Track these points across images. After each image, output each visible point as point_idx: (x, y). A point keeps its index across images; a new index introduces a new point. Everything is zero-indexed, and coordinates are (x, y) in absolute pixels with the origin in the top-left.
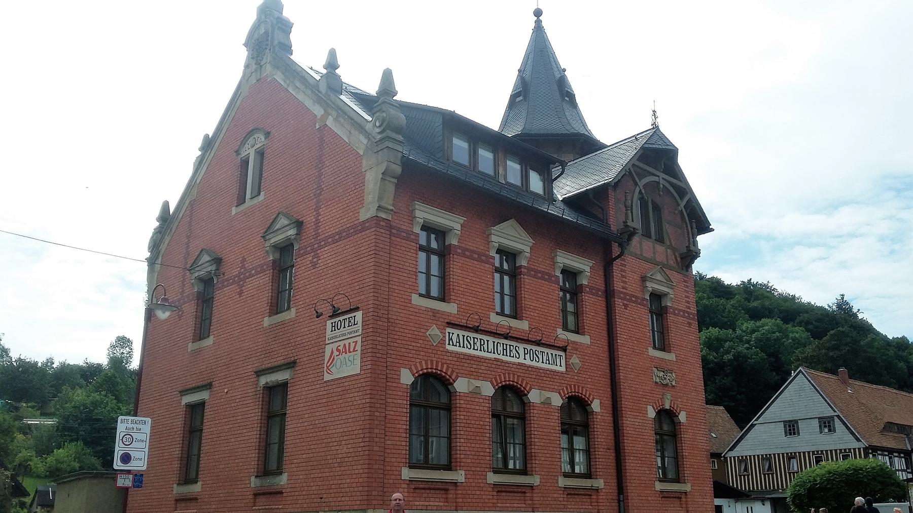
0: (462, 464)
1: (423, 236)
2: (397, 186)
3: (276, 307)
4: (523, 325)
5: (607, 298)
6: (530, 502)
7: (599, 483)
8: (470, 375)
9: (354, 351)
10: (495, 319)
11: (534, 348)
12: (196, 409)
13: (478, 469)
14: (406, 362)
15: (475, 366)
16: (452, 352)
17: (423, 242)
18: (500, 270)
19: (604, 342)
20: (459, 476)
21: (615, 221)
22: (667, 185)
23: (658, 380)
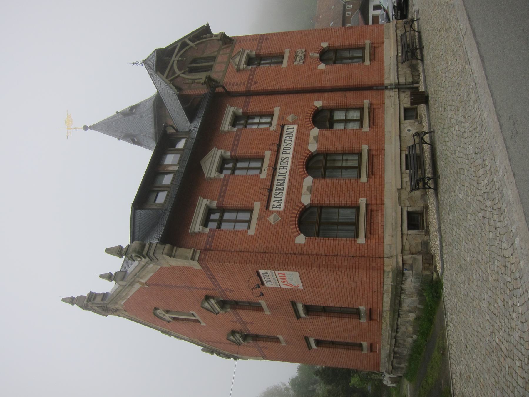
0: (356, 200)
1: (227, 172)
2: (180, 246)
3: (258, 308)
4: (268, 154)
5: (251, 95)
6: (379, 151)
7: (366, 103)
8: (299, 194)
10: (263, 176)
11: (282, 147)
12: (318, 343)
13: (358, 188)
14: (291, 239)
15: (294, 190)
16: (285, 206)
17: (228, 172)
18: (234, 169)
19: (279, 98)
20: (363, 202)
21: (203, 90)
22: (179, 55)
23: (302, 61)
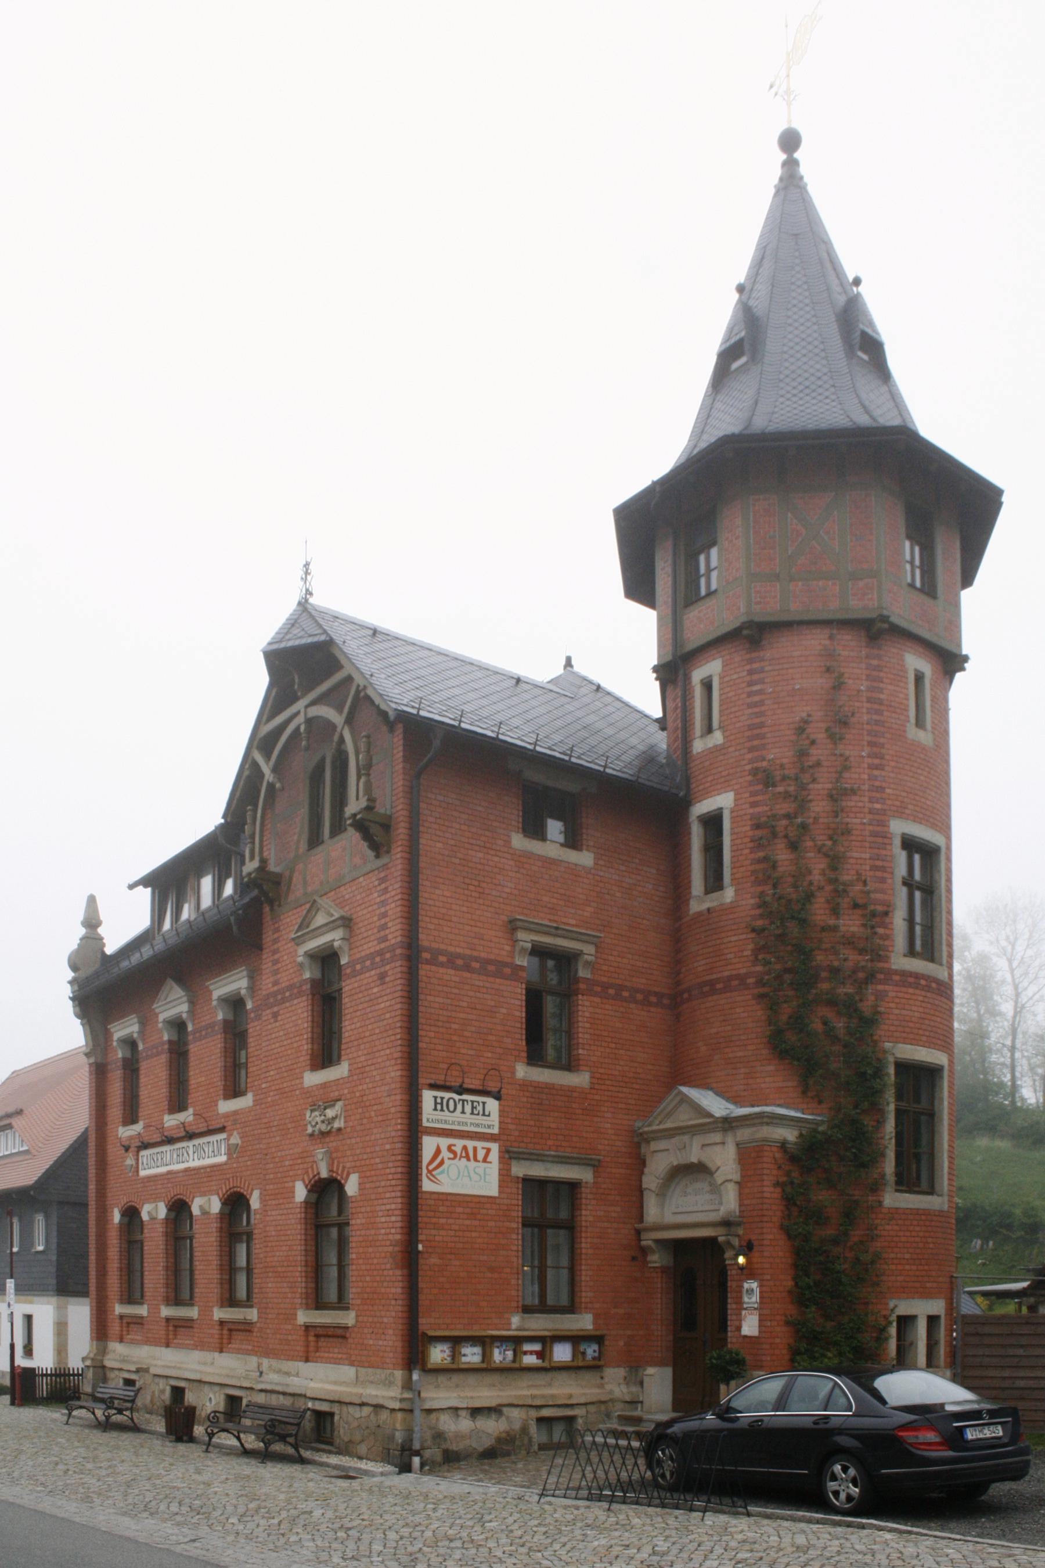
9: (485, 1160)
